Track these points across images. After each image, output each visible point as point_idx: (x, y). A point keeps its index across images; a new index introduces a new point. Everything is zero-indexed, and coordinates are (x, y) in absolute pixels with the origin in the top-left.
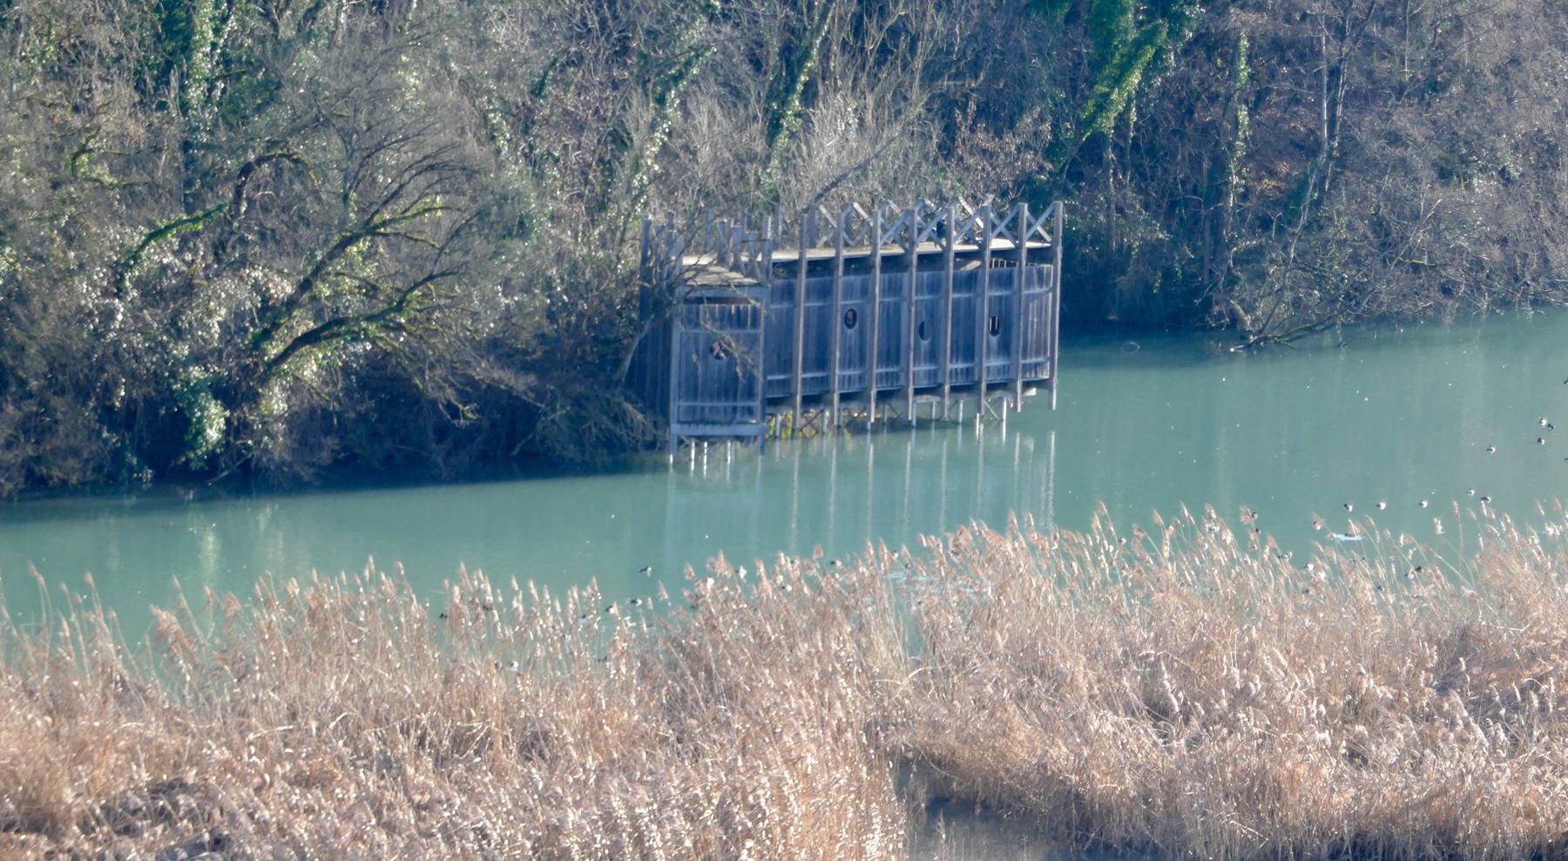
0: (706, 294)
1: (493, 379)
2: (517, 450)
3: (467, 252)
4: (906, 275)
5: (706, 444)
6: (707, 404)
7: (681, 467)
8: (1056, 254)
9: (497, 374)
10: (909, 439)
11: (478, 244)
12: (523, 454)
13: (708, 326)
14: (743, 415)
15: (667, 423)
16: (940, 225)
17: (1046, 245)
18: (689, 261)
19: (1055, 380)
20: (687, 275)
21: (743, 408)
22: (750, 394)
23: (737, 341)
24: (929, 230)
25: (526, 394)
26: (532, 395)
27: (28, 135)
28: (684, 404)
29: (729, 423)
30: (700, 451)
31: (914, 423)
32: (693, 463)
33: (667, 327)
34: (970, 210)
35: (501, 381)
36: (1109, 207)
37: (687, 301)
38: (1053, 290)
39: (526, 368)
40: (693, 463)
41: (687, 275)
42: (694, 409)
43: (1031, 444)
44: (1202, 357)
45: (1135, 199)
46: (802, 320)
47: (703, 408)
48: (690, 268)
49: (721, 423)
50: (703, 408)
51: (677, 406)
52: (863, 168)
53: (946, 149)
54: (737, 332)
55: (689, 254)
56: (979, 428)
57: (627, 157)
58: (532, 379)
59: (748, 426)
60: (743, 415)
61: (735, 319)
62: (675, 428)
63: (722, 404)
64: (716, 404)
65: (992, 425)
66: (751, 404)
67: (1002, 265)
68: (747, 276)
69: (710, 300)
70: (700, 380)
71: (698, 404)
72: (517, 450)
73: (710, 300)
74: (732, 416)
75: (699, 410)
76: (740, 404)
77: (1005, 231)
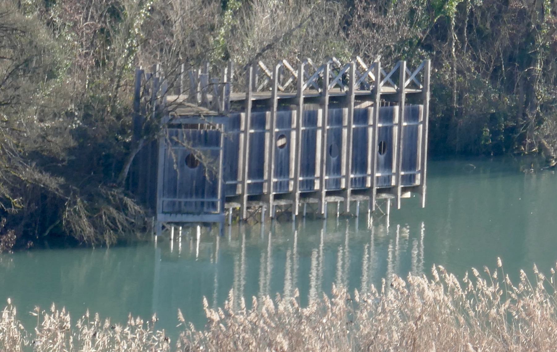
0: (183, 121)
1: (35, 180)
2: (48, 232)
3: (17, 88)
4: (268, 113)
5: (181, 228)
6: (183, 200)
7: (164, 242)
8: (425, 98)
9: (37, 176)
10: (321, 227)
11: (24, 82)
12: (51, 234)
13: (185, 144)
14: (208, 208)
15: (155, 213)
16: (344, 76)
17: (418, 91)
18: (170, 98)
19: (424, 188)
20: (170, 109)
21: (209, 203)
22: (214, 193)
23: (205, 154)
24: (337, 79)
25: (57, 190)
26: (61, 191)
27: (250, 322)
28: (167, 200)
29: (199, 214)
30: (176, 230)
31: (325, 216)
32: (172, 242)
33: (155, 145)
34: (364, 66)
35: (40, 180)
36: (452, 69)
37: (171, 126)
38: (424, 122)
39: (55, 172)
40: (172, 242)
41: (170, 109)
42: (174, 203)
43: (407, 232)
44: (516, 171)
45: (471, 63)
46: (396, 148)
47: (180, 203)
48: (171, 104)
49: (193, 213)
50: (180, 203)
51: (162, 201)
52: (289, 34)
53: (346, 24)
54: (205, 148)
55: (170, 94)
56: (370, 221)
57: (120, 26)
58: (62, 180)
59: (212, 216)
60: (208, 208)
61: (203, 138)
62: (160, 216)
63: (194, 199)
64: (189, 200)
65: (379, 218)
66: (214, 200)
67: (387, 105)
68: (211, 110)
69: (186, 126)
70: (178, 183)
71: (177, 200)
72: (48, 232)
73: (186, 126)
74: (201, 208)
75: (177, 204)
76: (206, 200)
77: (390, 81)
